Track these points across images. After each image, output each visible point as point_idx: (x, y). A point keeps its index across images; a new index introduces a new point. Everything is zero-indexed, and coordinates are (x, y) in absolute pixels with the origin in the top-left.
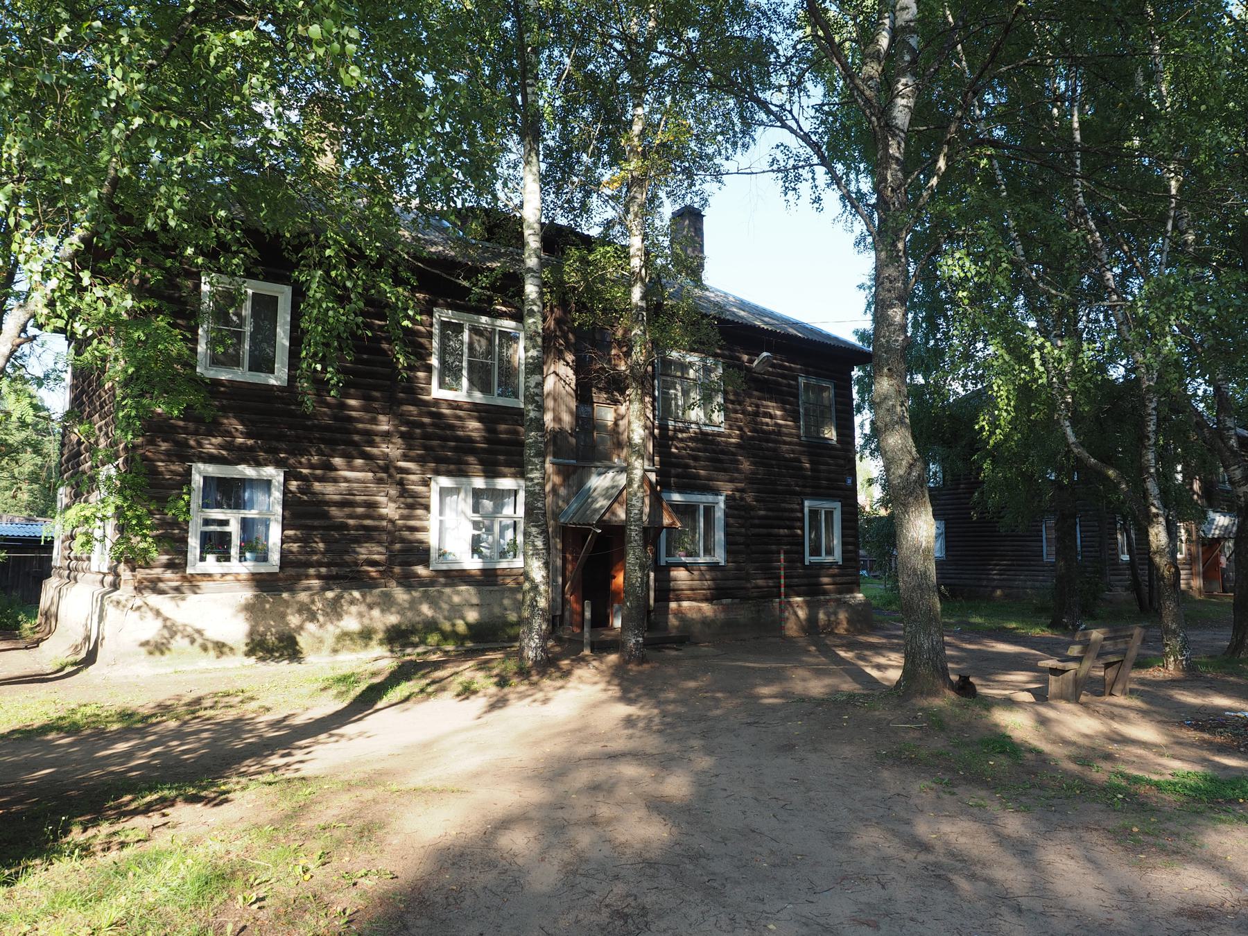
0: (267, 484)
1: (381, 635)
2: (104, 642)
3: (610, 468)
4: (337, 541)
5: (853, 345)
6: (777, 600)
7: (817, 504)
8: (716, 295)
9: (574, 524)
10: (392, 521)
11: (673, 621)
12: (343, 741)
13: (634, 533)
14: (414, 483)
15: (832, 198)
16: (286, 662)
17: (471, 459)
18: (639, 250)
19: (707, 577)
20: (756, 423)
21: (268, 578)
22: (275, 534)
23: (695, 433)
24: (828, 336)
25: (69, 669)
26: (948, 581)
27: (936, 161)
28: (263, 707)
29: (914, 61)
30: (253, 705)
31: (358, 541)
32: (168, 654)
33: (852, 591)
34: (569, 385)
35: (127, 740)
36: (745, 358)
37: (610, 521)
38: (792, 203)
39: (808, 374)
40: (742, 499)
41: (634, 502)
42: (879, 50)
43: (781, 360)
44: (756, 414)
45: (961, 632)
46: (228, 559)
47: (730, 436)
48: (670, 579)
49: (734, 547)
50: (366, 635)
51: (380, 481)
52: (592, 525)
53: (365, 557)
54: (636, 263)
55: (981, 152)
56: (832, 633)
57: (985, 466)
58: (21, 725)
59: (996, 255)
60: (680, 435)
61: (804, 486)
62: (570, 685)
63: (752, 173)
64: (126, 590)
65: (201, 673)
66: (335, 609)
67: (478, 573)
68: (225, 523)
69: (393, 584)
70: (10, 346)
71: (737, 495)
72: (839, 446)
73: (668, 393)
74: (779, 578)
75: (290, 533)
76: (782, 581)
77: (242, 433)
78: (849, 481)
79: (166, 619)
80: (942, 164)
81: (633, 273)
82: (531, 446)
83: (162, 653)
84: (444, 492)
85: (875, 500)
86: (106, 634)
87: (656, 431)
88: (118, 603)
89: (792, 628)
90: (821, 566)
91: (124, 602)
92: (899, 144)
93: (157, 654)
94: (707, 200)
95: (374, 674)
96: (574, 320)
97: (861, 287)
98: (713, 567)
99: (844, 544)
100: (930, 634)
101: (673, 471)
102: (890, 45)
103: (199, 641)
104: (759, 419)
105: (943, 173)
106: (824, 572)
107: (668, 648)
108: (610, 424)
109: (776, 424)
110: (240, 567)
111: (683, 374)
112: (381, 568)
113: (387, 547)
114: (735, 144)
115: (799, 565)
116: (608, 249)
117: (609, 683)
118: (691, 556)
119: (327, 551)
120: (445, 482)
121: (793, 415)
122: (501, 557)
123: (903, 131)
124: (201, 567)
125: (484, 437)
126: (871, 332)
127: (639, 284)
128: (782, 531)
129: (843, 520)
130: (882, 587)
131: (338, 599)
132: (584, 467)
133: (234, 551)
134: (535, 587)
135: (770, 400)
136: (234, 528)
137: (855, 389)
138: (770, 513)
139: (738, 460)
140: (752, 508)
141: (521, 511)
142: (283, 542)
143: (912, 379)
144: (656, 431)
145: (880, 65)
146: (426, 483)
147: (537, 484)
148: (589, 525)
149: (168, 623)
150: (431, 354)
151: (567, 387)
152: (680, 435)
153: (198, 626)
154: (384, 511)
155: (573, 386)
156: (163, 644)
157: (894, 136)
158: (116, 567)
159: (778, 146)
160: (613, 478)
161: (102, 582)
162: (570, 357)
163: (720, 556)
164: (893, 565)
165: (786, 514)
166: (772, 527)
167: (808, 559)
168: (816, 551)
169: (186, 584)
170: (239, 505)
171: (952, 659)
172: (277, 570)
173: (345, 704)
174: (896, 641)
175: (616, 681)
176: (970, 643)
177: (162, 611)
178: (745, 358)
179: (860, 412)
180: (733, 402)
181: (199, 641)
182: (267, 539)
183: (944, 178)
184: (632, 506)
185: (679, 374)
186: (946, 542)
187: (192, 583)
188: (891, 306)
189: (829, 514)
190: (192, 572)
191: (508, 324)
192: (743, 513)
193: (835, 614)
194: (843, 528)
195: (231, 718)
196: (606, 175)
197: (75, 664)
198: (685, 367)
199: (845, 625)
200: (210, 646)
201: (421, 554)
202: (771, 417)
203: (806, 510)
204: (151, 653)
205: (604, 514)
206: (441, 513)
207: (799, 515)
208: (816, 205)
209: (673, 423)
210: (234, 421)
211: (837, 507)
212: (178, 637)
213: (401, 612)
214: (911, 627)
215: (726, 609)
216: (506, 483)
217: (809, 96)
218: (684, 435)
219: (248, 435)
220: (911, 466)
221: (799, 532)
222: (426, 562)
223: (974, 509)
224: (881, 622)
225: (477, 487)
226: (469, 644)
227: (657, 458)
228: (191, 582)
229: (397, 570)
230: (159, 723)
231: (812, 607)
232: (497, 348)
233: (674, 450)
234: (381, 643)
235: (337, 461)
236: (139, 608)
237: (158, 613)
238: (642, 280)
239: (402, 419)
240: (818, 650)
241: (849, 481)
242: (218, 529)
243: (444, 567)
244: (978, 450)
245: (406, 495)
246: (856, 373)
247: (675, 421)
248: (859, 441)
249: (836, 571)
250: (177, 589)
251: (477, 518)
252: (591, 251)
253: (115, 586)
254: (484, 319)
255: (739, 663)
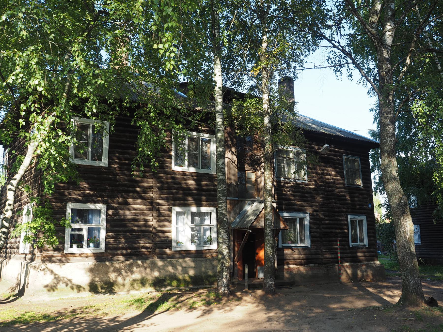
0: (99, 212)
1: (150, 282)
2: (29, 285)
3: (255, 201)
4: (130, 238)
5: (369, 140)
6: (337, 265)
7: (354, 217)
8: (301, 118)
9: (238, 228)
10: (155, 228)
11: (286, 275)
12: (145, 327)
13: (268, 231)
14: (164, 210)
15: (356, 73)
16: (109, 294)
17: (190, 198)
18: (267, 100)
19: (302, 253)
20: (323, 178)
21: (100, 255)
22: (103, 235)
23: (293, 184)
24: (357, 136)
25: (12, 298)
26: (423, 256)
27: (406, 59)
28: (105, 313)
29: (393, 15)
30: (100, 312)
31: (139, 237)
32: (56, 291)
33: (374, 260)
34: (234, 163)
35: (51, 327)
36: (316, 147)
37: (256, 226)
38: (339, 77)
39: (347, 154)
40: (317, 215)
41: (268, 217)
42: (377, 10)
43: (333, 148)
44: (323, 174)
45: (431, 281)
46: (82, 247)
47: (310, 185)
48: (283, 254)
49: (315, 239)
50: (143, 282)
51: (150, 210)
52: (247, 228)
53: (142, 245)
54: (266, 106)
55: (426, 56)
56: (365, 281)
57: (438, 197)
58: (3, 320)
59: (436, 102)
60: (286, 185)
61: (347, 208)
62: (242, 304)
63: (321, 68)
64: (38, 262)
65: (71, 299)
66: (130, 269)
67: (194, 252)
68: (80, 230)
69: (156, 257)
70: (31, 158)
71: (315, 213)
72: (363, 188)
73: (280, 165)
74: (338, 253)
75: (110, 234)
76: (339, 255)
77: (88, 189)
78: (370, 206)
79: (55, 275)
80: (408, 61)
81: (264, 111)
82: (220, 192)
83: (54, 290)
84: (178, 214)
85: (383, 215)
86: (30, 282)
87: (275, 183)
88: (35, 267)
89: (344, 278)
90: (358, 247)
91: (37, 267)
92: (388, 52)
93: (52, 291)
94: (297, 76)
95: (152, 299)
96: (237, 133)
97: (371, 110)
98: (305, 248)
99: (369, 236)
100: (414, 277)
101: (284, 202)
102: (382, 8)
103: (70, 285)
104: (324, 176)
105: (409, 65)
106: (359, 251)
107: (285, 288)
108: (253, 180)
109: (333, 179)
110: (89, 250)
111: (287, 156)
112: (149, 250)
113: (152, 240)
114: (309, 49)
115: (347, 247)
116: (253, 100)
117: (259, 303)
118: (294, 243)
119: (126, 242)
120: (177, 209)
121: (340, 174)
122: (204, 245)
123: (389, 46)
124: (71, 251)
125: (196, 188)
126: (377, 132)
127: (267, 116)
128: (338, 231)
129: (368, 225)
130: (389, 259)
131: (131, 265)
132: (242, 201)
133: (85, 243)
134: (224, 258)
135: (329, 167)
136: (85, 233)
137: (371, 160)
138: (331, 222)
139: (314, 197)
140: (323, 220)
141: (214, 222)
142: (106, 238)
143: (399, 154)
144: (275, 183)
145: (377, 16)
146: (170, 210)
147: (224, 209)
148: (246, 228)
149: (56, 276)
150: (171, 150)
151: (233, 164)
152: (286, 185)
153: (69, 278)
154: (151, 223)
155: (236, 163)
156: (54, 286)
157: (385, 48)
158: (33, 251)
159: (331, 52)
160: (256, 206)
161: (25, 258)
162: (233, 149)
163: (307, 243)
164: (394, 248)
165: (339, 222)
166: (332, 228)
167: (351, 244)
168: (355, 240)
169: (63, 258)
170: (86, 221)
171: (426, 293)
172: (103, 251)
173: (141, 312)
174: (398, 285)
175: (263, 302)
176: (435, 286)
177: (54, 271)
178: (316, 147)
179: (373, 171)
180: (311, 169)
181: (70, 285)
182: (99, 238)
183: (409, 67)
184: (267, 219)
185: (285, 156)
186: (421, 236)
187: (65, 259)
188: (387, 125)
189: (361, 222)
190: (67, 253)
191: (206, 136)
192: (318, 222)
193: (366, 271)
194: (368, 229)
195: (92, 318)
196: (249, 66)
197: (14, 296)
198: (287, 152)
199: (371, 276)
200: (75, 287)
201: (168, 243)
202: (330, 175)
203: (349, 220)
204: (49, 291)
205: (253, 223)
206: (177, 223)
207: (346, 222)
208: (350, 78)
209: (283, 179)
210: (84, 183)
211: (364, 219)
212: (61, 283)
213: (159, 269)
214: (404, 273)
215: (311, 269)
216: (204, 209)
217: (344, 30)
218: (289, 185)
219: (90, 189)
220: (401, 199)
221: (346, 231)
222: (170, 247)
223: (434, 218)
224: (389, 276)
225: (193, 211)
226: (191, 286)
227: (276, 196)
228: (66, 257)
229: (157, 251)
230: (61, 319)
231: (354, 268)
232: (201, 147)
233: (284, 192)
234: (151, 285)
235: (130, 200)
236: (44, 269)
237: (52, 272)
238: (269, 114)
239: (159, 180)
240: (359, 289)
241: (370, 206)
242: (77, 232)
243: (178, 249)
244: (434, 189)
245: (161, 216)
246: (371, 152)
247: (284, 178)
248: (374, 186)
249: (365, 250)
250: (60, 261)
251: (193, 226)
252: (244, 101)
253: (32, 260)
254: (195, 134)
255: (321, 295)
